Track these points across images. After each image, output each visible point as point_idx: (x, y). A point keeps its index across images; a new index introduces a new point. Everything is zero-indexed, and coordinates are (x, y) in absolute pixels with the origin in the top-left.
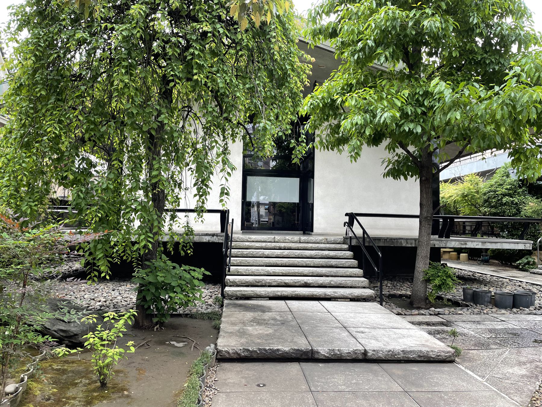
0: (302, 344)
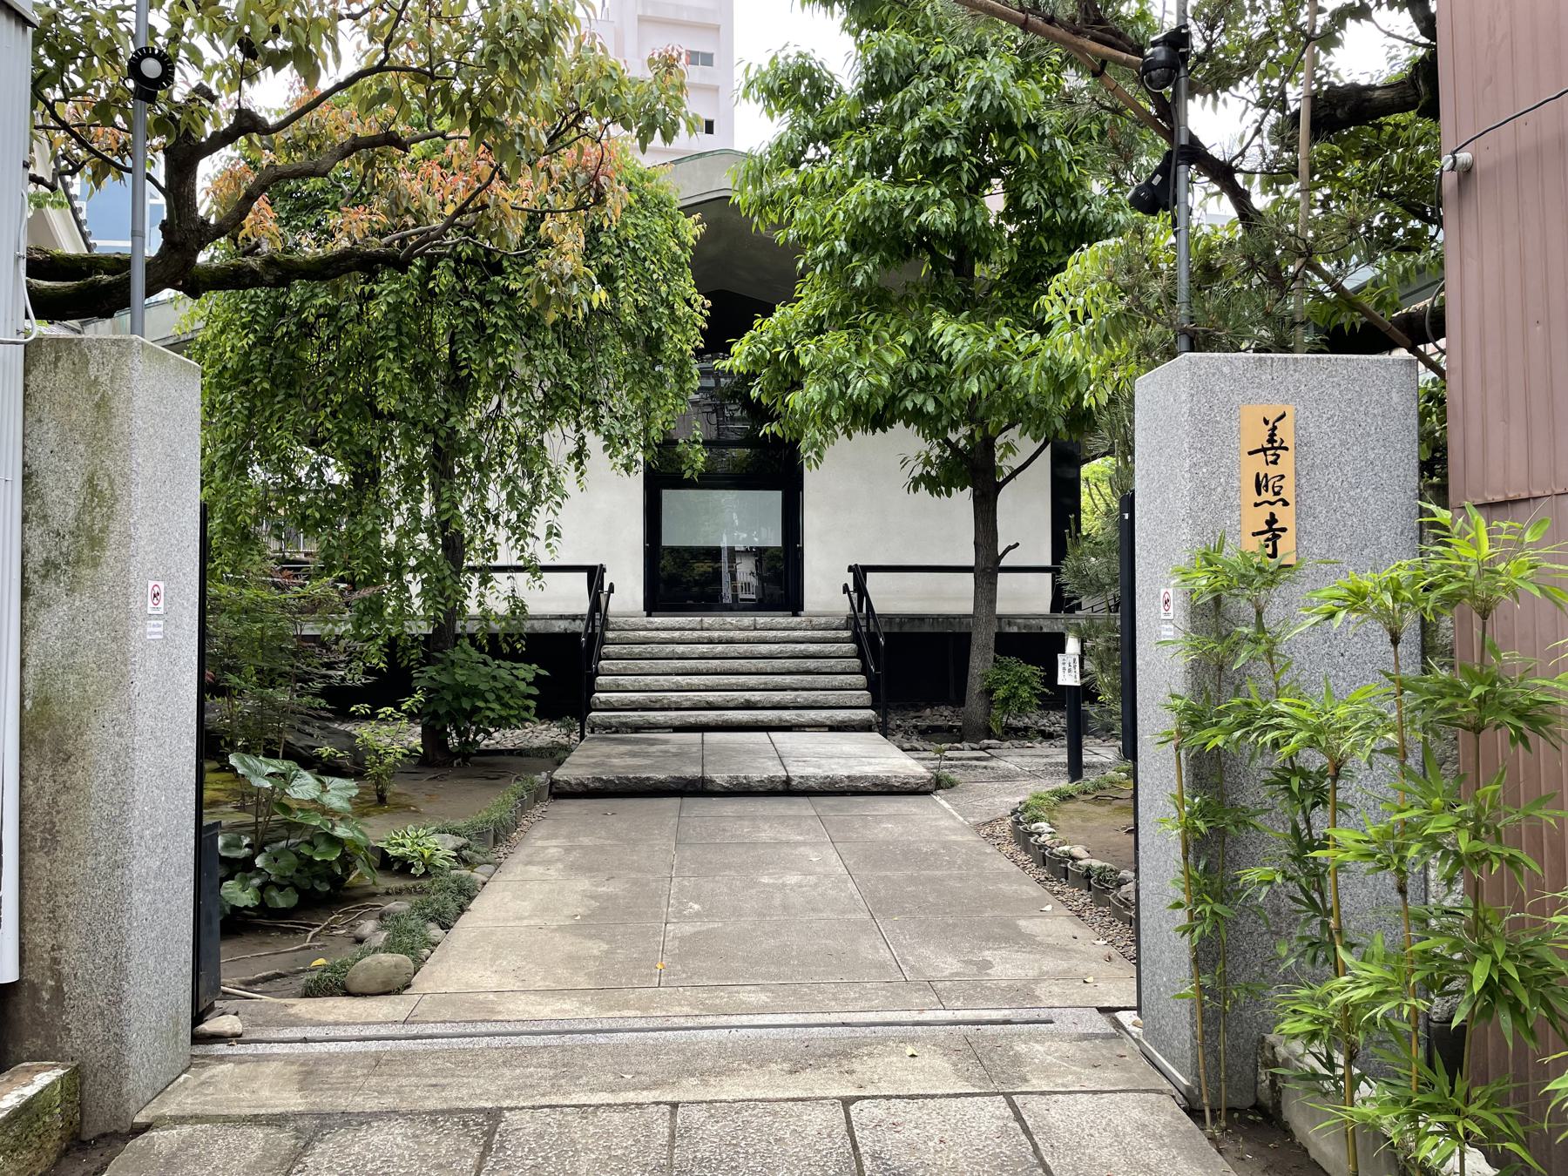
0: (692, 771)
